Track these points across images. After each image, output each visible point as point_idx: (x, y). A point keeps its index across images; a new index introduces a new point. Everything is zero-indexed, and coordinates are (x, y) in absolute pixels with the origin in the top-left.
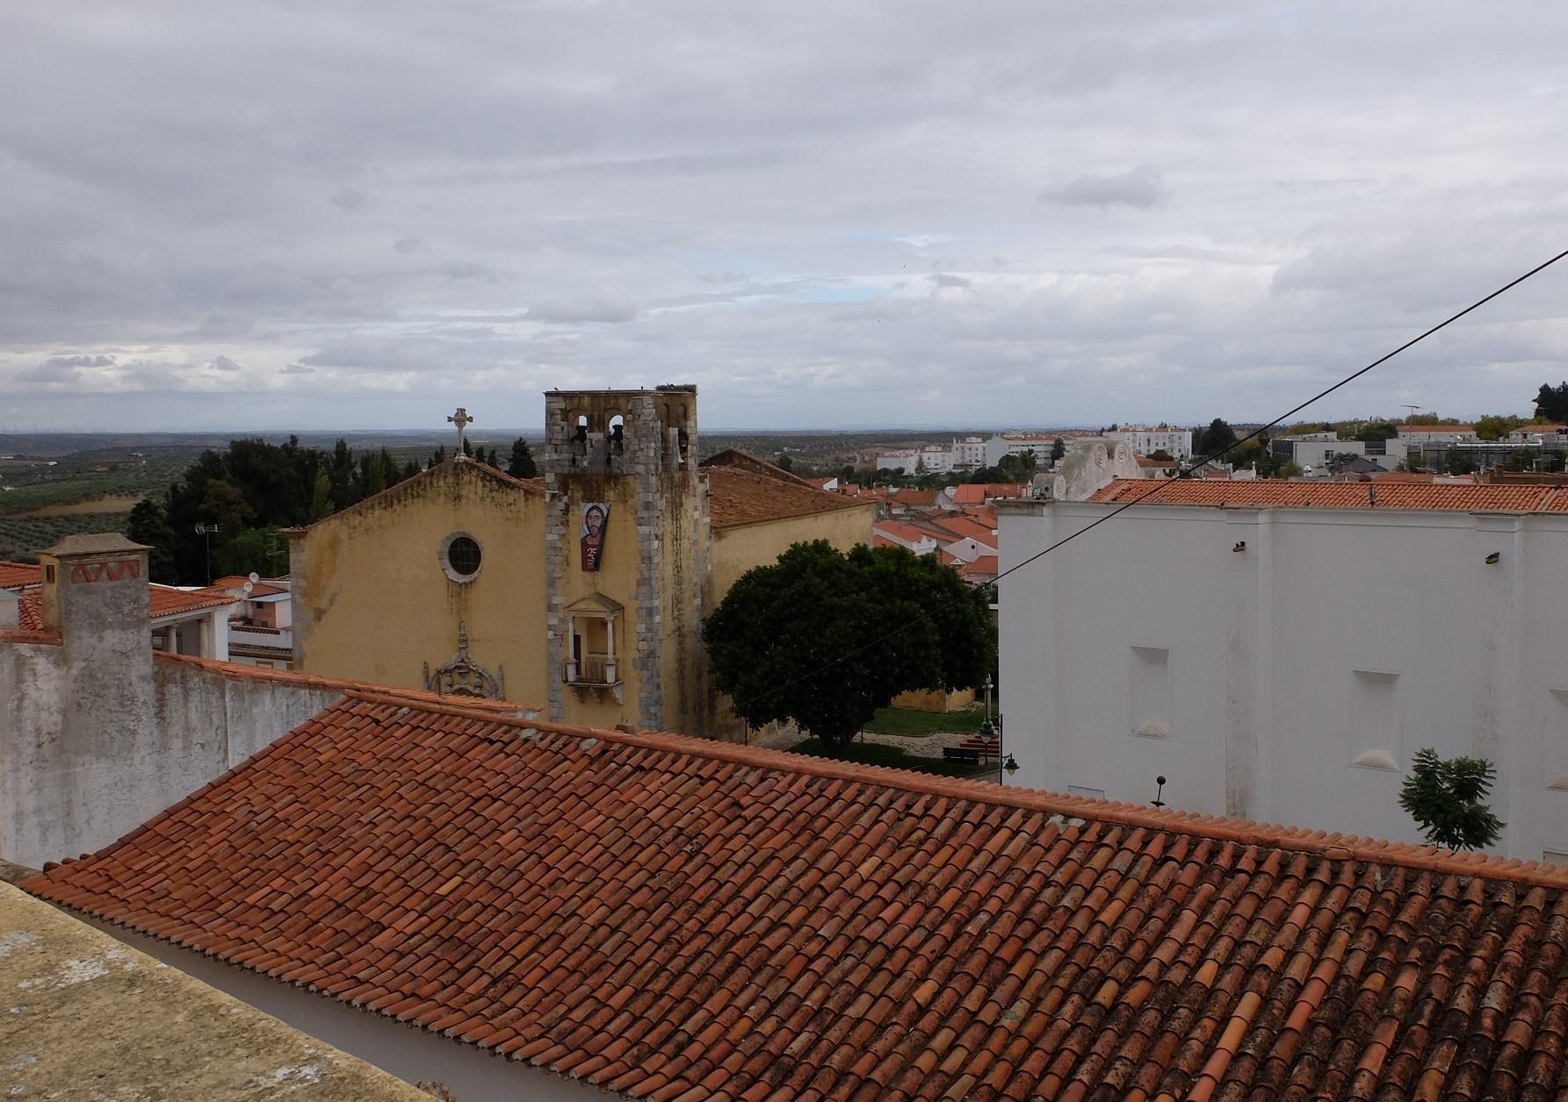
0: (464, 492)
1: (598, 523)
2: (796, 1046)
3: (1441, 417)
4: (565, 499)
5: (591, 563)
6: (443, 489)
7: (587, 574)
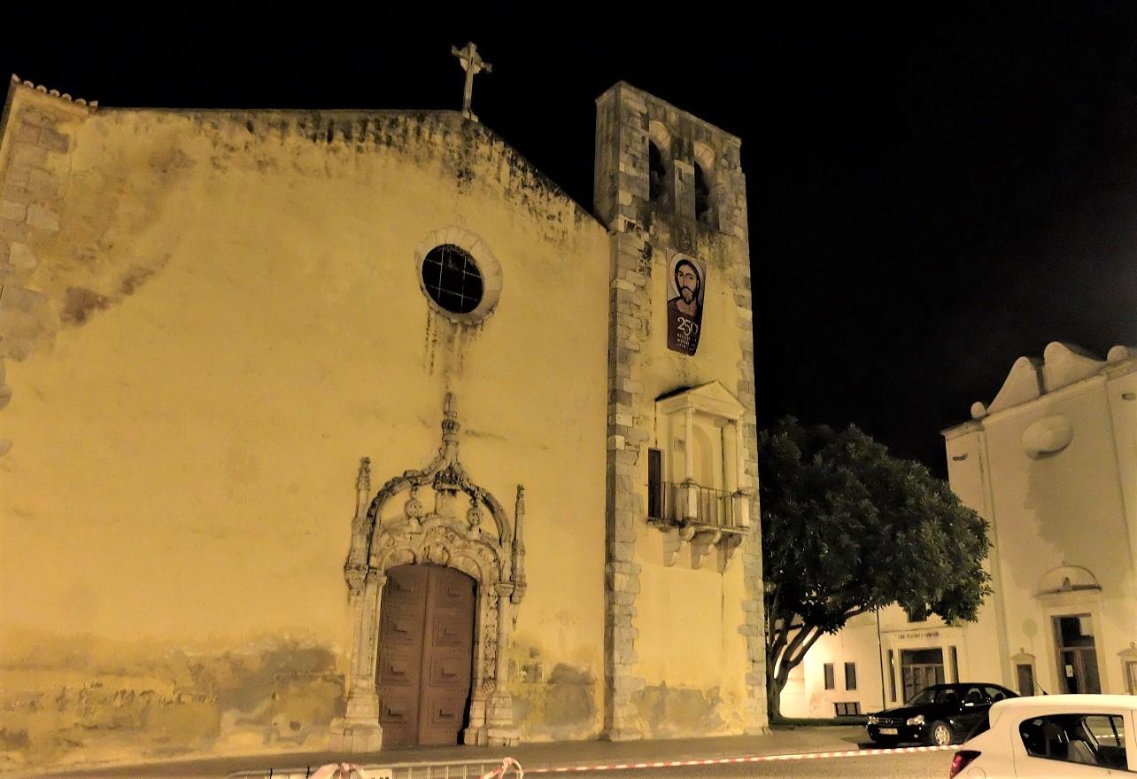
0: (478, 169)
1: (692, 285)
2: (611, 130)
3: (466, 730)
4: (646, 236)
5: (685, 340)
6: (439, 149)
7: (675, 355)
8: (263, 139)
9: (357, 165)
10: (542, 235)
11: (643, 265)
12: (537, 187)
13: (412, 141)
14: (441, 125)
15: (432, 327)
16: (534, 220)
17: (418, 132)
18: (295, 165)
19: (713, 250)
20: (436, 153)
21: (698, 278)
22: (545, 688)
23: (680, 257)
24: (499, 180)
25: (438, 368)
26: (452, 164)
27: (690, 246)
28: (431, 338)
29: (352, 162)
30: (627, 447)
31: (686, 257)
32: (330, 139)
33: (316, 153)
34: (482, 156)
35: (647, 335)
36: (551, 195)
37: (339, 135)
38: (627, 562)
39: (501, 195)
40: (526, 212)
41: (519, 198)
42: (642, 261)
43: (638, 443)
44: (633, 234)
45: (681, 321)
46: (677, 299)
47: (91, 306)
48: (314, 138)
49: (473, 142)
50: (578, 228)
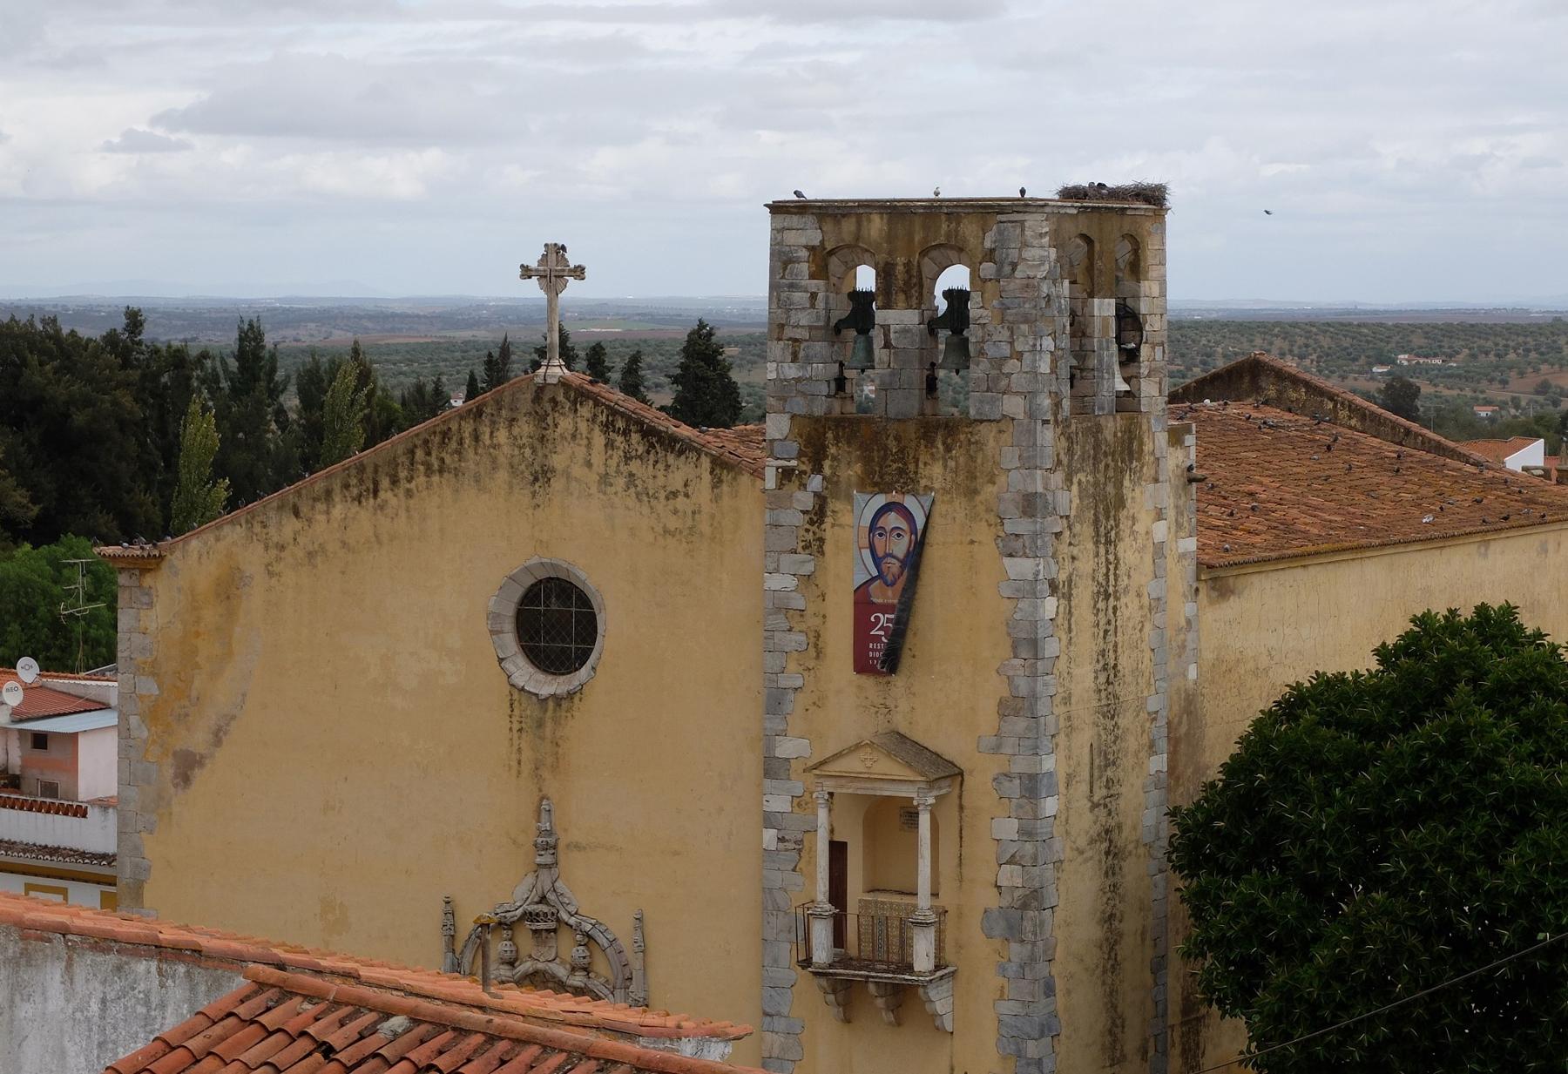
0: (557, 461)
1: (900, 547)
4: (816, 482)
5: (876, 652)
7: (868, 682)
8: (309, 521)
9: (409, 517)
10: (659, 529)
11: (810, 536)
12: (648, 452)
13: (470, 454)
14: (503, 412)
15: (516, 712)
16: (646, 510)
17: (476, 438)
18: (344, 544)
19: (952, 464)
20: (502, 460)
21: (913, 530)
22: (1549, 823)
23: (880, 500)
24: (589, 464)
25: (527, 768)
26: (523, 467)
27: (902, 472)
28: (516, 726)
29: (403, 514)
30: (781, 845)
31: (894, 497)
32: (376, 493)
33: (364, 517)
34: (563, 437)
35: (818, 657)
36: (671, 458)
37: (385, 482)
38: (779, 1014)
39: (594, 490)
40: (632, 501)
41: (621, 482)
42: (807, 530)
43: (799, 837)
44: (792, 487)
45: (877, 618)
46: (873, 579)
47: (192, 768)
48: (358, 499)
49: (549, 420)
50: (717, 499)
